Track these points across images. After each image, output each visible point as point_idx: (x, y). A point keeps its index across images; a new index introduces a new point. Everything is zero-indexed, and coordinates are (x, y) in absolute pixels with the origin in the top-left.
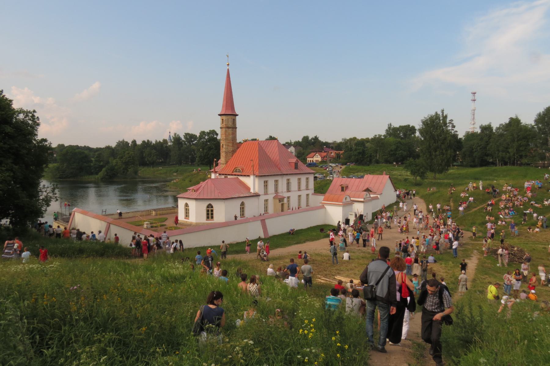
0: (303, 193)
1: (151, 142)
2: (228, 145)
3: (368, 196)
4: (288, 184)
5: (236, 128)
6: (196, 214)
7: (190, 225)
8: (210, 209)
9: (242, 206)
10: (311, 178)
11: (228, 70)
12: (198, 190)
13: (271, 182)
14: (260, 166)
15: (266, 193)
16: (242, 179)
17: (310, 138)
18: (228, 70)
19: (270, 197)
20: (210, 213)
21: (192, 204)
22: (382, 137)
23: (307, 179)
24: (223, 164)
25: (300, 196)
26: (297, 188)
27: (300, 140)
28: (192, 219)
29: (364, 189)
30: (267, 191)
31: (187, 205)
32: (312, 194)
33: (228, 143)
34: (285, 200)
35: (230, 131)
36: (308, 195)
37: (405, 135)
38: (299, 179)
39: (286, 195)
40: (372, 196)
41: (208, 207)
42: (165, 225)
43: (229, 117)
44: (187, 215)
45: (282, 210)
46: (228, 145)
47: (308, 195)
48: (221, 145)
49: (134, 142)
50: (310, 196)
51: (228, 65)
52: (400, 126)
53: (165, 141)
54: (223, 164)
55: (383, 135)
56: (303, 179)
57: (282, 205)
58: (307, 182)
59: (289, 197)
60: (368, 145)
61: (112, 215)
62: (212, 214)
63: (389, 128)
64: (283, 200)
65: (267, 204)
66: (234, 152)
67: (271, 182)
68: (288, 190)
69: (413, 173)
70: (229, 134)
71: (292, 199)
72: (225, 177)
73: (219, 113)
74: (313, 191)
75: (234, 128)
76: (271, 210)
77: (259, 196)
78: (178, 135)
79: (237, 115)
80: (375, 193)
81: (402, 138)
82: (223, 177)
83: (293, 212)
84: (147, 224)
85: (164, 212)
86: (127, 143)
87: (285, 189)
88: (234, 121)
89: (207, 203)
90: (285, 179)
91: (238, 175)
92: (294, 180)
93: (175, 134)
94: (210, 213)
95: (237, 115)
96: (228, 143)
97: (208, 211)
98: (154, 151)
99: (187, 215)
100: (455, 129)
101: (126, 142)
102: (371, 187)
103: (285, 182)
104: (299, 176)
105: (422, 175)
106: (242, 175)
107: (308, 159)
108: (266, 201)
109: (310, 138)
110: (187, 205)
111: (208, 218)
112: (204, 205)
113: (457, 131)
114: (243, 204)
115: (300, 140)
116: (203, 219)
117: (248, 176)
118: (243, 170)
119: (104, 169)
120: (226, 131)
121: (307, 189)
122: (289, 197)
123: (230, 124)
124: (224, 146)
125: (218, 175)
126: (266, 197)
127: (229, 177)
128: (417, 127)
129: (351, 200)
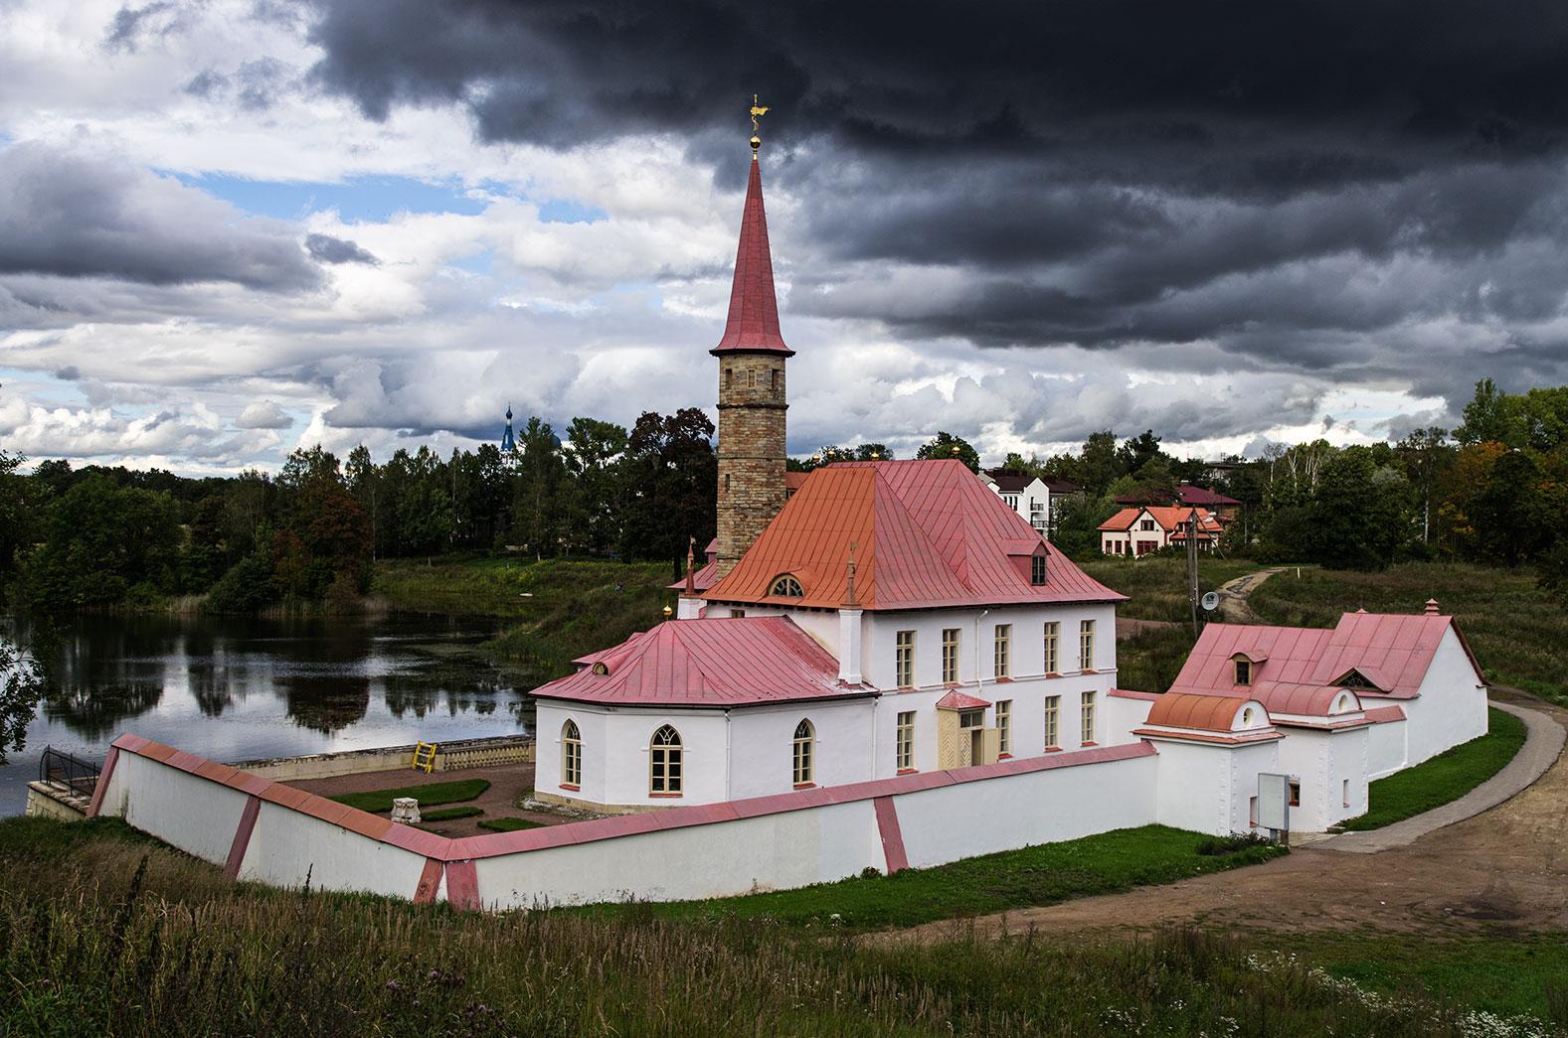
2: (750, 480)
4: (1051, 645)
7: (585, 813)
8: (667, 748)
9: (802, 741)
10: (1106, 627)
16: (804, 623)
17: (1119, 444)
20: (667, 763)
22: (1450, 442)
26: (1076, 666)
33: (752, 469)
34: (990, 717)
41: (657, 740)
42: (482, 812)
44: (573, 774)
48: (722, 477)
54: (726, 559)
56: (1069, 626)
58: (1087, 641)
62: (676, 770)
73: (714, 347)
76: (927, 759)
80: (1384, 694)
92: (1027, 634)
95: (791, 354)
96: (752, 469)
99: (573, 774)
101: (329, 457)
106: (803, 609)
107: (1106, 537)
110: (571, 729)
111: (658, 784)
117: (832, 611)
120: (740, 422)
121: (1086, 669)
122: (1004, 705)
123: (760, 391)
126: (905, 703)
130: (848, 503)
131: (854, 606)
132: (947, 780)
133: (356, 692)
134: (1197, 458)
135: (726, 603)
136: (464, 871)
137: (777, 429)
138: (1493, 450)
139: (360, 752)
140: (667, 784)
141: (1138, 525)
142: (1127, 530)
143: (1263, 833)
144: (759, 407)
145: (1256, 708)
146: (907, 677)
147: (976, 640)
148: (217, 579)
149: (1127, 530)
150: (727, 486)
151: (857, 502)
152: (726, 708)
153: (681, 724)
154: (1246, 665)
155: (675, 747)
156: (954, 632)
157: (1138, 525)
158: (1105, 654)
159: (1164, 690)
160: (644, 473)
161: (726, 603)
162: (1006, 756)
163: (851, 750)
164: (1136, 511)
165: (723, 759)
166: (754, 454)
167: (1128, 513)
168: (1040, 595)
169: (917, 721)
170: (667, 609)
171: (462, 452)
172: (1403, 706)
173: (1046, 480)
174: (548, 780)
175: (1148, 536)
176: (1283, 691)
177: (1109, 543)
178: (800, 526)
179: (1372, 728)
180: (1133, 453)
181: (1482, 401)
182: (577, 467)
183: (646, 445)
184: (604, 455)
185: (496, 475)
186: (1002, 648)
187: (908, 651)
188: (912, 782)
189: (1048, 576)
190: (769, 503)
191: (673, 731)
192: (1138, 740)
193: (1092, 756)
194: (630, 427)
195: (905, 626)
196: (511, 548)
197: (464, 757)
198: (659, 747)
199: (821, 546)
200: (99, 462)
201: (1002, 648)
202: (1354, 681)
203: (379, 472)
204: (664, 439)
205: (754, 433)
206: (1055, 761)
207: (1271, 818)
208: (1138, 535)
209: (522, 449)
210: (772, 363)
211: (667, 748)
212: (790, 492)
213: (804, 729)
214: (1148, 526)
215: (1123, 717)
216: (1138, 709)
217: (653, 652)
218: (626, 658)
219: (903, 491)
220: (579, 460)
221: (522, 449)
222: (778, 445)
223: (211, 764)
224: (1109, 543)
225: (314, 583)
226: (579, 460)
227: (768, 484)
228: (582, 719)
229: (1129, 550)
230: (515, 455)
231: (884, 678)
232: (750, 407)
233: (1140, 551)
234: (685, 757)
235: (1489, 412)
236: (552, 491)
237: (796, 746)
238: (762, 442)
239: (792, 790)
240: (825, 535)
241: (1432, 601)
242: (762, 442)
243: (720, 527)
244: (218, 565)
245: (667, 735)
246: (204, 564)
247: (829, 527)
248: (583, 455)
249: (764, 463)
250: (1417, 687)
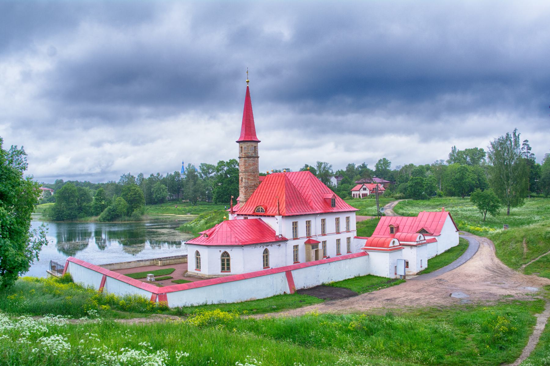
0: (343, 237)
2: (248, 179)
3: (422, 238)
5: (258, 157)
7: (201, 278)
8: (226, 258)
9: (265, 255)
10: (353, 218)
11: (248, 87)
12: (211, 234)
13: (302, 223)
14: (289, 204)
15: (295, 238)
16: (266, 220)
17: (356, 166)
18: (248, 87)
19: (301, 243)
20: (226, 262)
21: (204, 253)
23: (348, 218)
24: (242, 202)
25: (338, 240)
26: (345, 230)
28: (205, 271)
29: (419, 229)
30: (296, 235)
31: (198, 253)
32: (355, 237)
33: (249, 176)
34: (320, 246)
35: (251, 161)
36: (349, 239)
37: (473, 159)
38: (337, 220)
39: (321, 239)
40: (427, 238)
41: (223, 255)
42: (172, 278)
43: (249, 144)
44: (198, 267)
45: (317, 258)
46: (248, 179)
47: (349, 239)
48: (240, 178)
50: (352, 239)
51: (248, 82)
52: (466, 150)
53: (177, 174)
54: (242, 202)
55: (446, 160)
56: (343, 218)
57: (317, 252)
59: (324, 242)
60: (428, 173)
61: (110, 265)
62: (228, 264)
63: (453, 151)
64: (317, 247)
65: (297, 251)
66: (256, 186)
67: (302, 223)
68: (324, 234)
69: (481, 207)
70: (249, 165)
71: (328, 244)
72: (245, 218)
73: (237, 140)
74: (355, 234)
75: (256, 157)
76: (302, 258)
78: (193, 166)
79: (259, 142)
80: (432, 235)
81: (469, 165)
82: (242, 218)
83: (329, 260)
84: (151, 276)
85: (173, 262)
88: (256, 148)
89: (223, 250)
91: (261, 216)
92: (330, 221)
93: (189, 165)
94: (226, 262)
95: (259, 142)
96: (249, 176)
97: (223, 261)
98: (163, 186)
99: (198, 267)
100: (531, 152)
101: (132, 177)
102: (427, 227)
103: (304, 225)
104: (337, 216)
105: (493, 209)
106: (265, 216)
107: (353, 193)
108: (296, 247)
109: (356, 166)
110: (198, 253)
111: (223, 269)
112: (217, 254)
113: (533, 154)
114: (266, 251)
115: (345, 170)
116: (217, 270)
117: (273, 216)
118: (266, 209)
119: (106, 209)
120: (245, 162)
121: (348, 231)
122: (324, 242)
123: (251, 153)
124: (244, 180)
125: (236, 215)
127: (249, 218)
128: (486, 150)
129: (400, 245)
130: (277, 185)
131: (280, 215)
132: (305, 266)
133: (141, 243)
134: (280, 168)
135: (242, 215)
136: (163, 297)
137: (256, 164)
138: (457, 166)
139: (138, 261)
140: (226, 268)
141: (362, 189)
143: (398, 277)
144: (251, 157)
145: (396, 240)
148: (102, 211)
149: (359, 190)
150: (242, 181)
151: (280, 184)
153: (228, 250)
154: (393, 228)
155: (228, 258)
156: (296, 223)
157: (362, 189)
158: (353, 226)
159: (370, 236)
160: (221, 179)
161: (242, 215)
162: (350, 252)
163: (280, 256)
164: (361, 185)
165: (245, 260)
166: (250, 171)
167: (359, 186)
170: (225, 217)
172: (436, 238)
173: (336, 177)
174: (191, 268)
175: (365, 192)
176: (404, 235)
177: (354, 194)
178: (263, 192)
179: (428, 245)
180: (360, 169)
182: (202, 177)
183: (220, 170)
184: (210, 173)
185: (179, 180)
188: (297, 265)
189: (336, 205)
190: (255, 185)
193: (350, 256)
194: (216, 165)
195: (294, 220)
196: (184, 201)
197: (168, 261)
198: (223, 258)
199: (270, 197)
200: (71, 179)
202: (423, 231)
203: (146, 180)
204: (226, 168)
205: (249, 165)
206: (340, 257)
207: (401, 271)
208: (362, 192)
209: (186, 173)
210: (254, 144)
211: (226, 258)
212: (260, 182)
213: (266, 251)
214: (365, 189)
215: (360, 244)
216: (363, 242)
217: (221, 230)
218: (213, 232)
219: (293, 181)
220: (203, 175)
221: (186, 173)
222: (257, 169)
223: (94, 266)
224: (354, 194)
225: (128, 213)
226: (203, 175)
227: (254, 180)
229: (360, 197)
230: (185, 174)
231: (288, 234)
232: (248, 157)
233: (363, 197)
235: (455, 155)
236: (195, 184)
237: (264, 256)
238: (251, 168)
239: (263, 270)
240: (271, 194)
242: (251, 168)
243: (240, 193)
244: (103, 207)
246: (99, 207)
247: (272, 192)
248: (204, 173)
249: (253, 174)
250: (440, 232)
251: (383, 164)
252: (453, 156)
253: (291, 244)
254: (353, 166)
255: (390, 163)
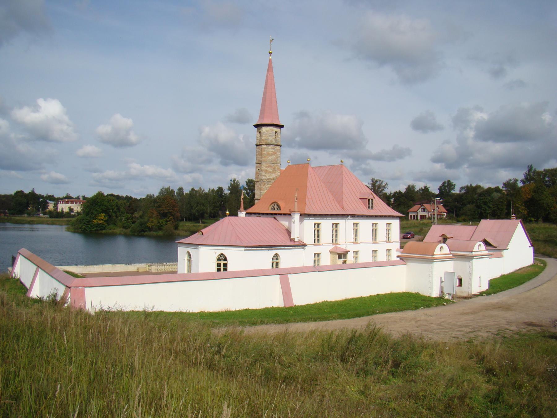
1: (204, 190)
4: (375, 231)
6: (213, 282)
9: (275, 262)
10: (396, 224)
22: (520, 184)
26: (384, 239)
27: (106, 194)
39: (351, 248)
41: (219, 259)
49: (181, 190)
53: (220, 190)
56: (382, 224)
58: (389, 230)
77: (305, 245)
86: (173, 191)
87: (350, 238)
90: (350, 222)
92: (365, 225)
106: (280, 214)
107: (410, 214)
114: (276, 257)
122: (356, 252)
126: (317, 249)
138: (533, 184)
141: (420, 210)
142: (416, 212)
144: (270, 145)
146: (318, 240)
147: (346, 225)
152: (246, 247)
155: (225, 262)
168: (371, 212)
169: (321, 256)
171: (212, 189)
181: (529, 171)
186: (356, 232)
187: (318, 231)
189: (374, 206)
191: (224, 256)
192: (399, 259)
198: (219, 262)
201: (356, 232)
205: (268, 154)
210: (275, 129)
211: (222, 262)
224: (411, 216)
228: (192, 251)
231: (308, 239)
234: (228, 265)
237: (273, 264)
241: (513, 215)
245: (222, 257)
251: (447, 186)
252: (529, 175)
253: (311, 250)
254: (413, 187)
255: (455, 185)
